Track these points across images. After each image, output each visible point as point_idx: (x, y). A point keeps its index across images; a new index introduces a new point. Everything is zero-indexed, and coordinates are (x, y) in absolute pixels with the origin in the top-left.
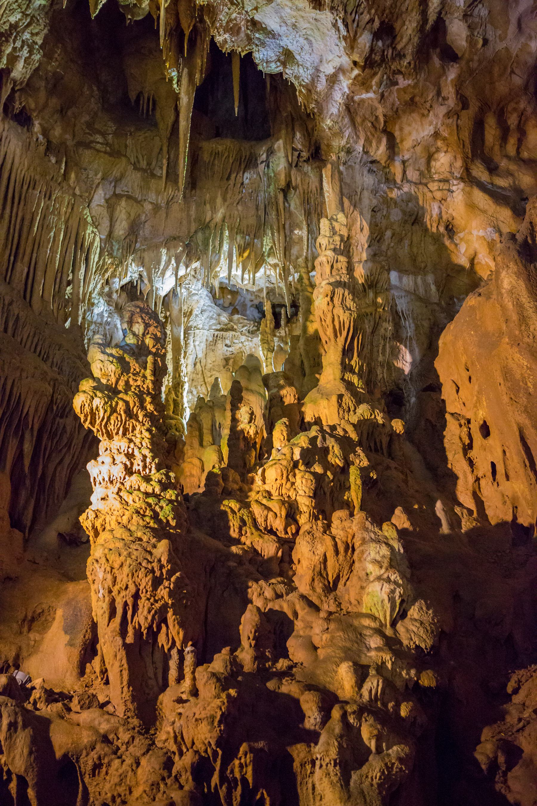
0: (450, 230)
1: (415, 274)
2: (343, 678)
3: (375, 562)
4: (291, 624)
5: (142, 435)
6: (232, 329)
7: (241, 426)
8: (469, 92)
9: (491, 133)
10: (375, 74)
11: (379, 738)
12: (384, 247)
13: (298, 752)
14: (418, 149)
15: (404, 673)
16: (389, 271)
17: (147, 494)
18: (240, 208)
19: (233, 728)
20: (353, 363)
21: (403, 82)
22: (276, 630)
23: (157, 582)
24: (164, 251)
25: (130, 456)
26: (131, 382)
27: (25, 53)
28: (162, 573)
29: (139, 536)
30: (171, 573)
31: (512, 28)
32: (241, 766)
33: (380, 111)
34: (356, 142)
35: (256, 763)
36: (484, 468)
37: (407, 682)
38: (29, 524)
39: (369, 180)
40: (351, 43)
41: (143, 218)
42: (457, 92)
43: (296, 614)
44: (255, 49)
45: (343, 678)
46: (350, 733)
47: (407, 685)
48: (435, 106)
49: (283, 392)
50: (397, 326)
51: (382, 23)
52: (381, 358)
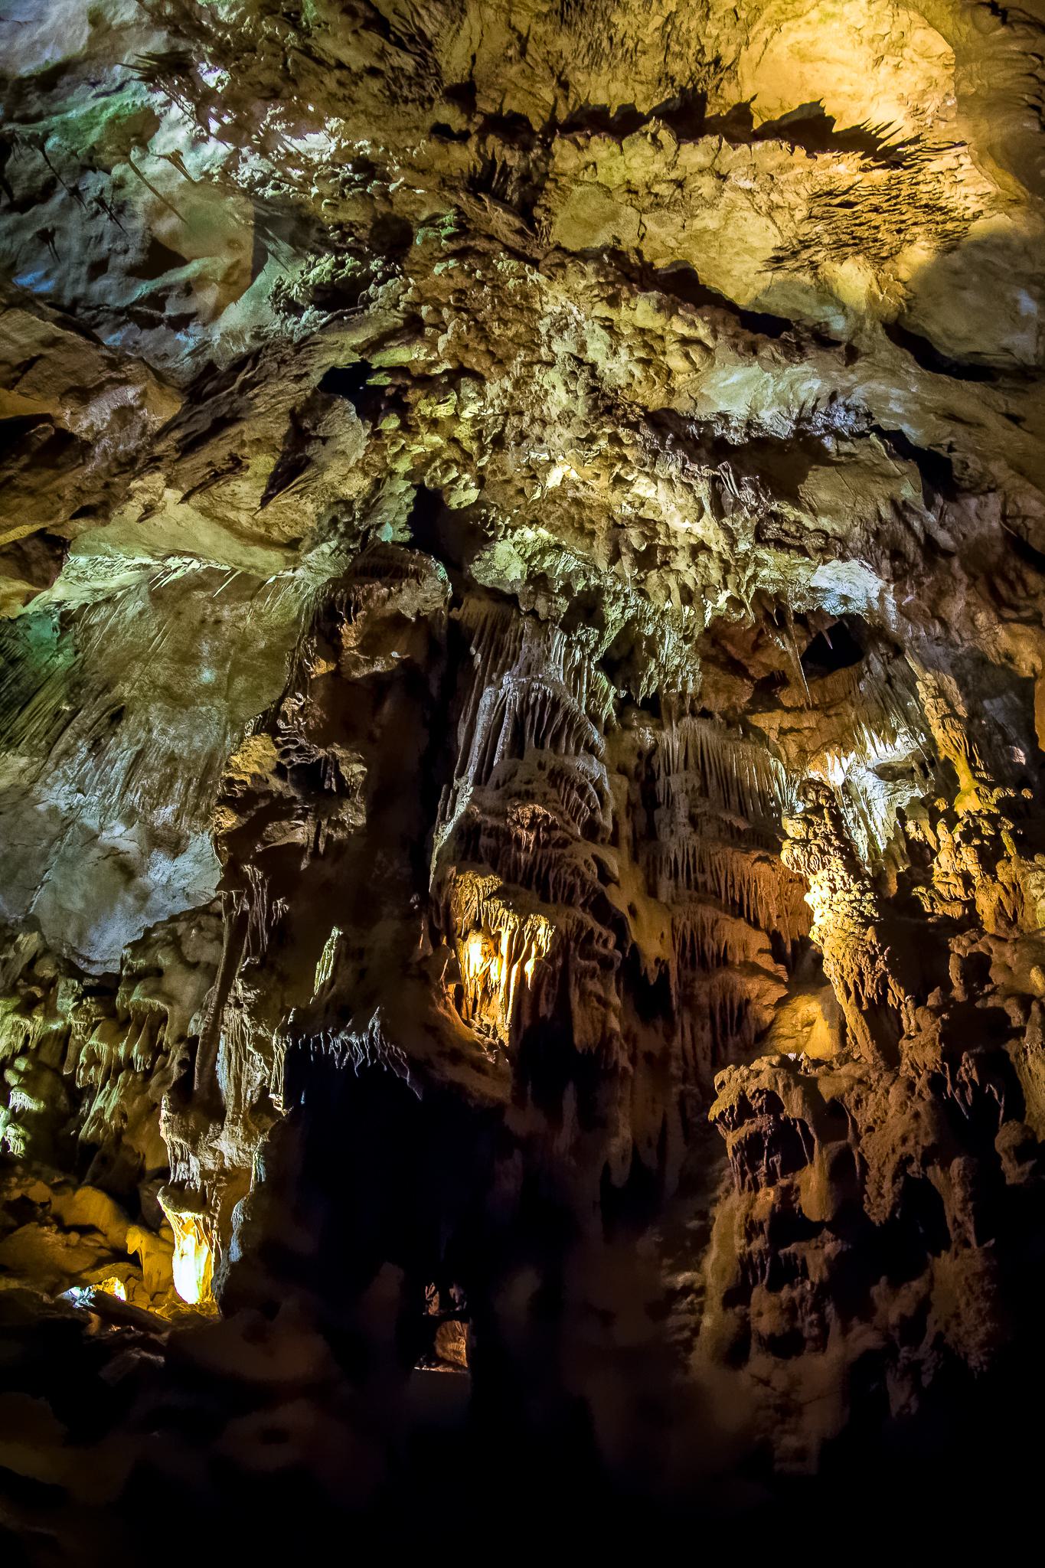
0: (1010, 658)
3: (1037, 886)
4: (989, 958)
5: (837, 863)
9: (1003, 589)
13: (1011, 1047)
17: (851, 902)
19: (951, 1044)
21: (927, 581)
22: (977, 968)
23: (873, 959)
25: (832, 880)
27: (691, 676)
29: (689, 829)
30: (882, 950)
31: (975, 521)
32: (967, 1071)
35: (977, 1065)
39: (940, 650)
40: (877, 569)
50: (1005, 735)
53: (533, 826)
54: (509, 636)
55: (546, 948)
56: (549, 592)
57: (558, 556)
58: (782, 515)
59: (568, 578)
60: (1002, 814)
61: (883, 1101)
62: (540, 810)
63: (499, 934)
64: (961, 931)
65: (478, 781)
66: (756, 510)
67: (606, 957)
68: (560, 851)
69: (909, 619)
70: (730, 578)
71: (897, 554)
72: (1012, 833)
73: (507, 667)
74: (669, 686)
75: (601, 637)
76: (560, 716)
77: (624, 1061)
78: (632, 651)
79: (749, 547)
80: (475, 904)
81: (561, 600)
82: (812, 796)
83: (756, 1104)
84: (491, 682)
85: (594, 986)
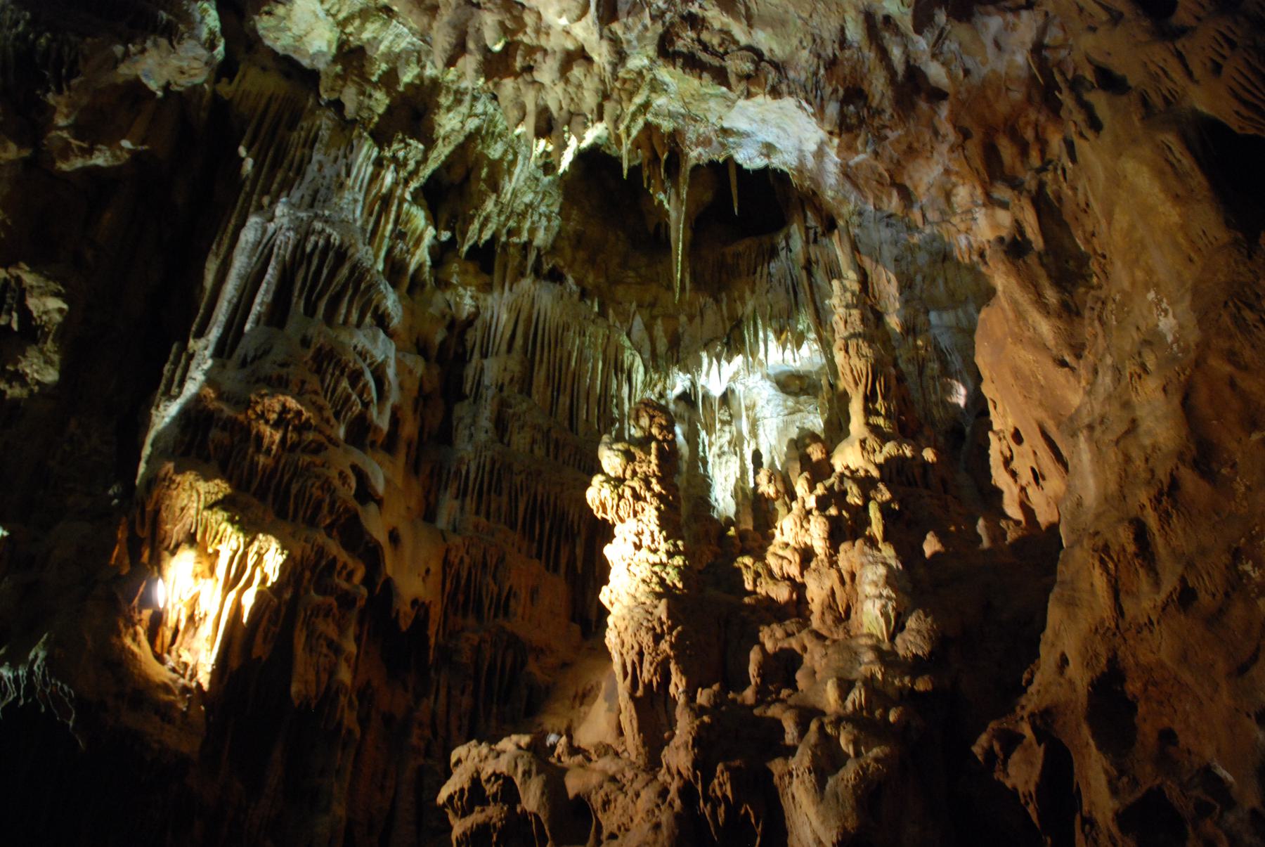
1: (954, 308)
2: (830, 696)
6: (800, 411)
7: (761, 490)
8: (967, 122)
9: (1007, 151)
10: (857, 136)
11: (856, 743)
12: (917, 291)
13: (777, 766)
14: (933, 190)
15: (897, 682)
16: (927, 312)
17: (654, 564)
18: (769, 295)
20: (878, 406)
21: (892, 135)
22: (784, 667)
23: (657, 639)
24: (704, 355)
25: (638, 534)
26: (638, 469)
27: (544, 222)
28: (663, 630)
30: (671, 629)
31: (991, 49)
32: (721, 785)
33: (881, 168)
34: (866, 203)
36: (1026, 477)
37: (900, 690)
38: (594, 619)
39: (886, 234)
40: (820, 114)
41: (681, 330)
42: (955, 127)
43: (805, 649)
44: (732, 152)
45: (830, 696)
46: (827, 744)
47: (901, 694)
48: (936, 145)
49: (810, 450)
51: (847, 90)
52: (933, 398)
53: (281, 422)
54: (296, 136)
55: (273, 578)
56: (364, 77)
57: (386, 24)
58: (704, 19)
59: (396, 61)
60: (882, 480)
61: (631, 805)
62: (292, 403)
63: (217, 553)
64: (780, 621)
65: (221, 351)
66: (663, 13)
67: (347, 593)
68: (307, 458)
69: (855, 185)
70: (609, 107)
71: (854, 94)
72: (884, 508)
73: (287, 186)
74: (511, 233)
75: (425, 159)
76: (345, 271)
77: (349, 719)
78: (467, 178)
79: (646, 62)
80: (193, 512)
81: (379, 95)
82: (645, 421)
83: (490, 789)
84: (260, 208)
85: (328, 628)
